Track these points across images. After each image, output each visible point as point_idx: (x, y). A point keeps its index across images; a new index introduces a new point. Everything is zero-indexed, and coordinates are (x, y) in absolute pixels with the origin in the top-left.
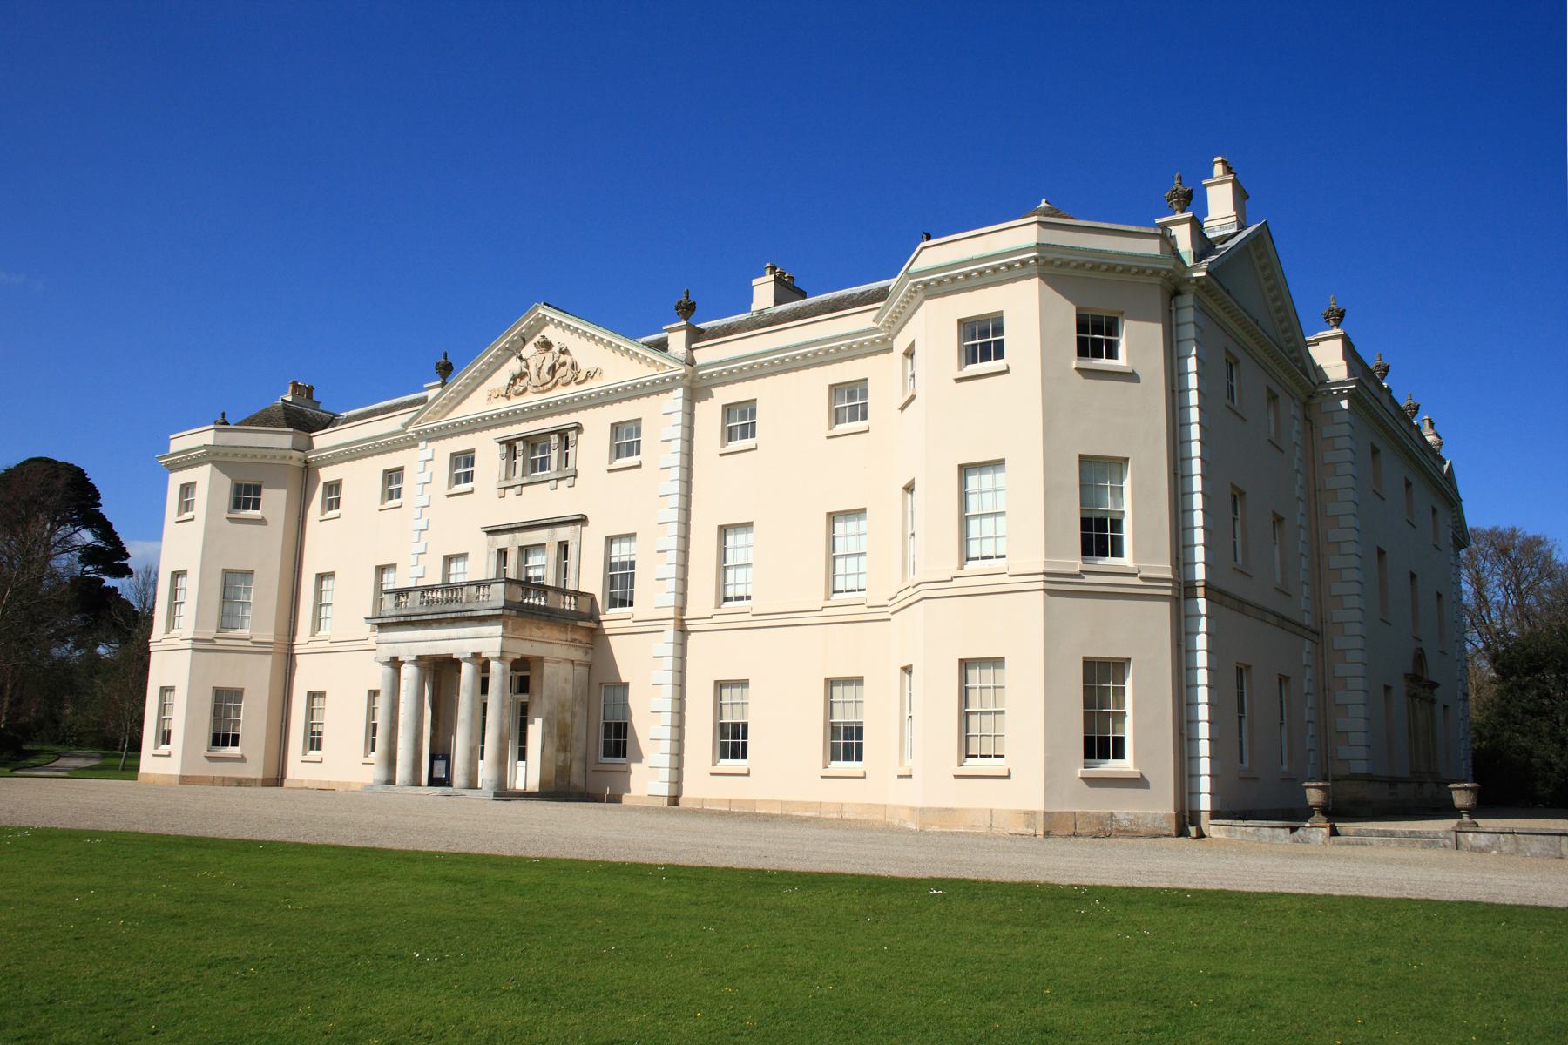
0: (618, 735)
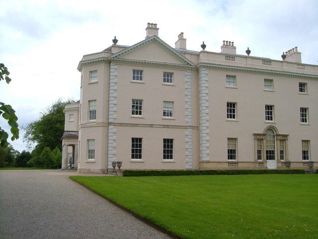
0: (305, 156)
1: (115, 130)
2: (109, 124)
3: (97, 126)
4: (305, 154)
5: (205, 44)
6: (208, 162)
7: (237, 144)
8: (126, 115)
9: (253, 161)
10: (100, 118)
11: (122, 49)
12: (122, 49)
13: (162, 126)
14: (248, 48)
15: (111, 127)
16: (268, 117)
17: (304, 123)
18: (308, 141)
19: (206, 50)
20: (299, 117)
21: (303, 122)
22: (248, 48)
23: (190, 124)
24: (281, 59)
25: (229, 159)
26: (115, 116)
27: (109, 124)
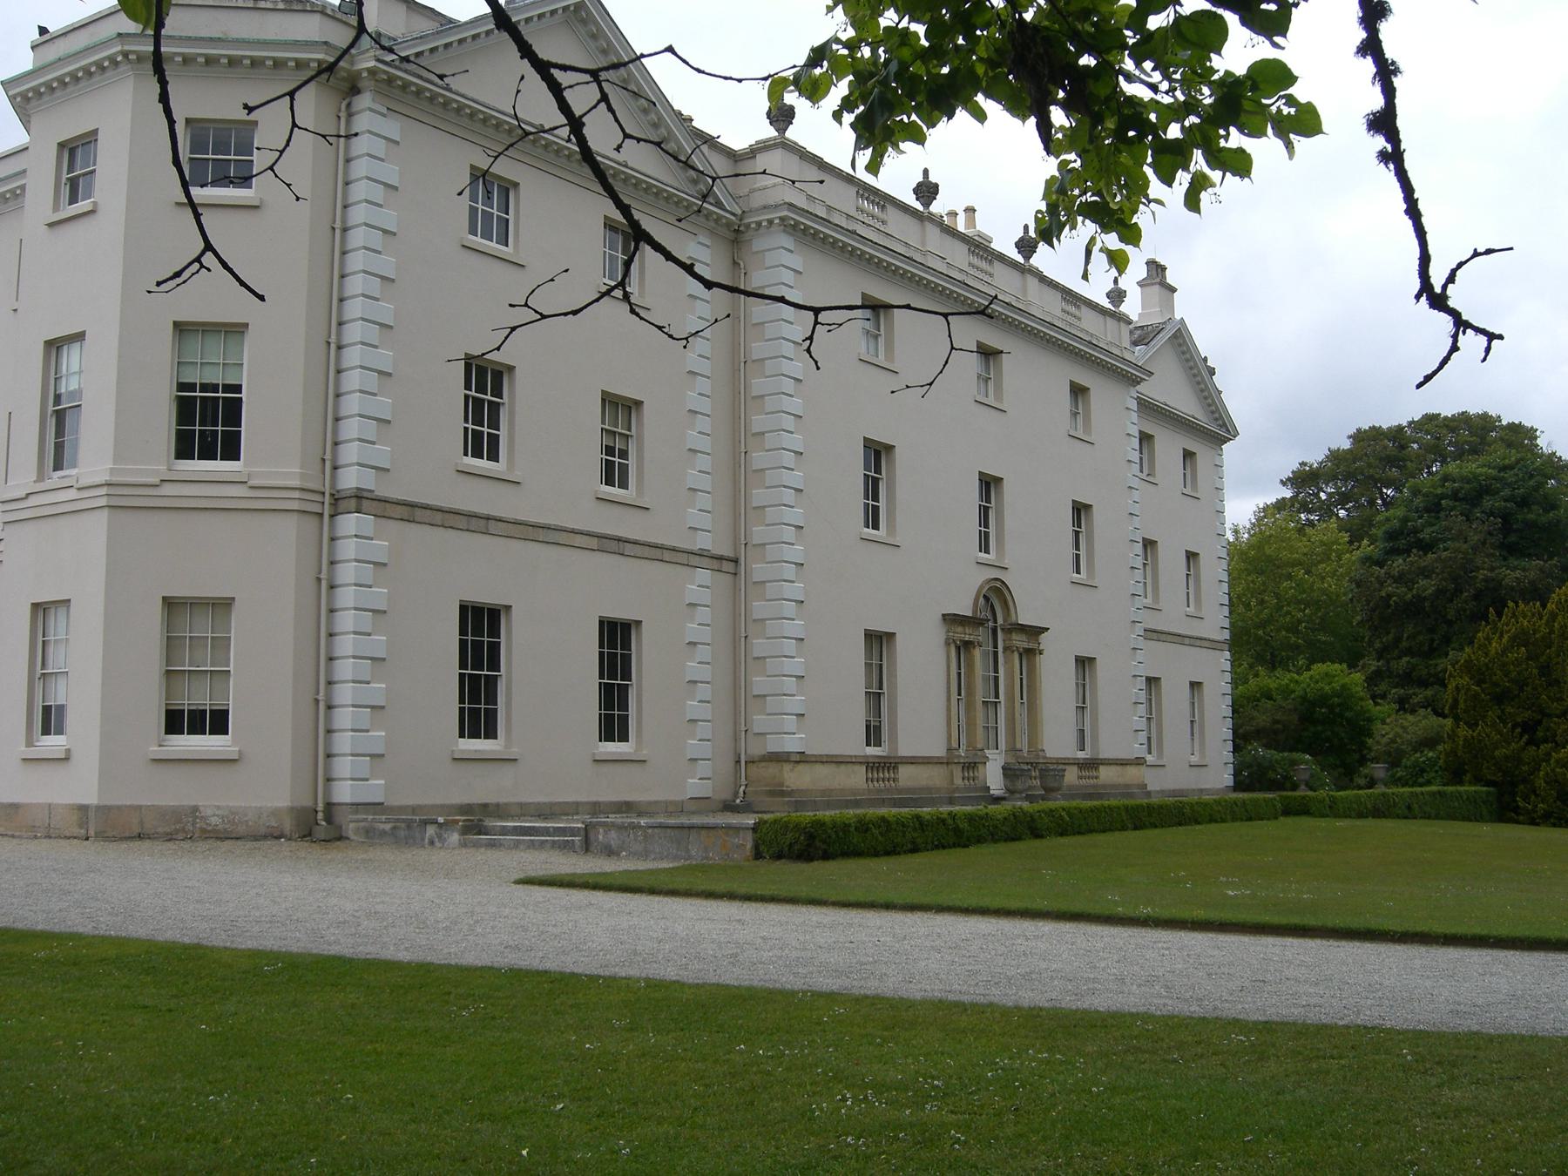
0: (475, 713)
1: (380, 547)
2: (339, 502)
3: (260, 504)
4: (475, 698)
5: (932, 178)
6: (802, 759)
7: (892, 663)
8: (433, 461)
9: (939, 751)
10: (272, 444)
11: (427, 26)
12: (427, 26)
13: (594, 543)
14: (926, 172)
15: (350, 523)
16: (478, 436)
17: (483, 464)
18: (1199, 684)
19: (792, 133)
20: (453, 423)
21: (477, 454)
22: (926, 172)
23: (703, 542)
24: (1105, 303)
25: (868, 744)
26: (381, 454)
27: (339, 502)
